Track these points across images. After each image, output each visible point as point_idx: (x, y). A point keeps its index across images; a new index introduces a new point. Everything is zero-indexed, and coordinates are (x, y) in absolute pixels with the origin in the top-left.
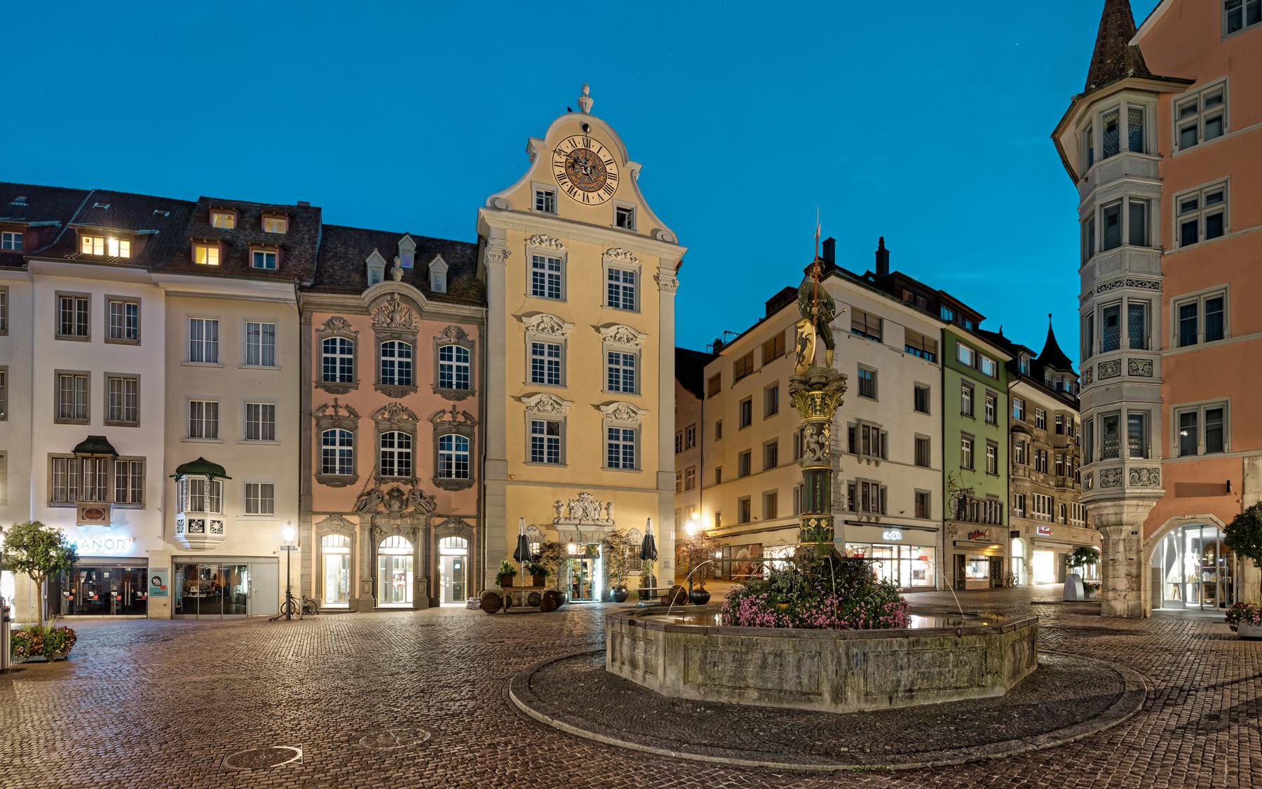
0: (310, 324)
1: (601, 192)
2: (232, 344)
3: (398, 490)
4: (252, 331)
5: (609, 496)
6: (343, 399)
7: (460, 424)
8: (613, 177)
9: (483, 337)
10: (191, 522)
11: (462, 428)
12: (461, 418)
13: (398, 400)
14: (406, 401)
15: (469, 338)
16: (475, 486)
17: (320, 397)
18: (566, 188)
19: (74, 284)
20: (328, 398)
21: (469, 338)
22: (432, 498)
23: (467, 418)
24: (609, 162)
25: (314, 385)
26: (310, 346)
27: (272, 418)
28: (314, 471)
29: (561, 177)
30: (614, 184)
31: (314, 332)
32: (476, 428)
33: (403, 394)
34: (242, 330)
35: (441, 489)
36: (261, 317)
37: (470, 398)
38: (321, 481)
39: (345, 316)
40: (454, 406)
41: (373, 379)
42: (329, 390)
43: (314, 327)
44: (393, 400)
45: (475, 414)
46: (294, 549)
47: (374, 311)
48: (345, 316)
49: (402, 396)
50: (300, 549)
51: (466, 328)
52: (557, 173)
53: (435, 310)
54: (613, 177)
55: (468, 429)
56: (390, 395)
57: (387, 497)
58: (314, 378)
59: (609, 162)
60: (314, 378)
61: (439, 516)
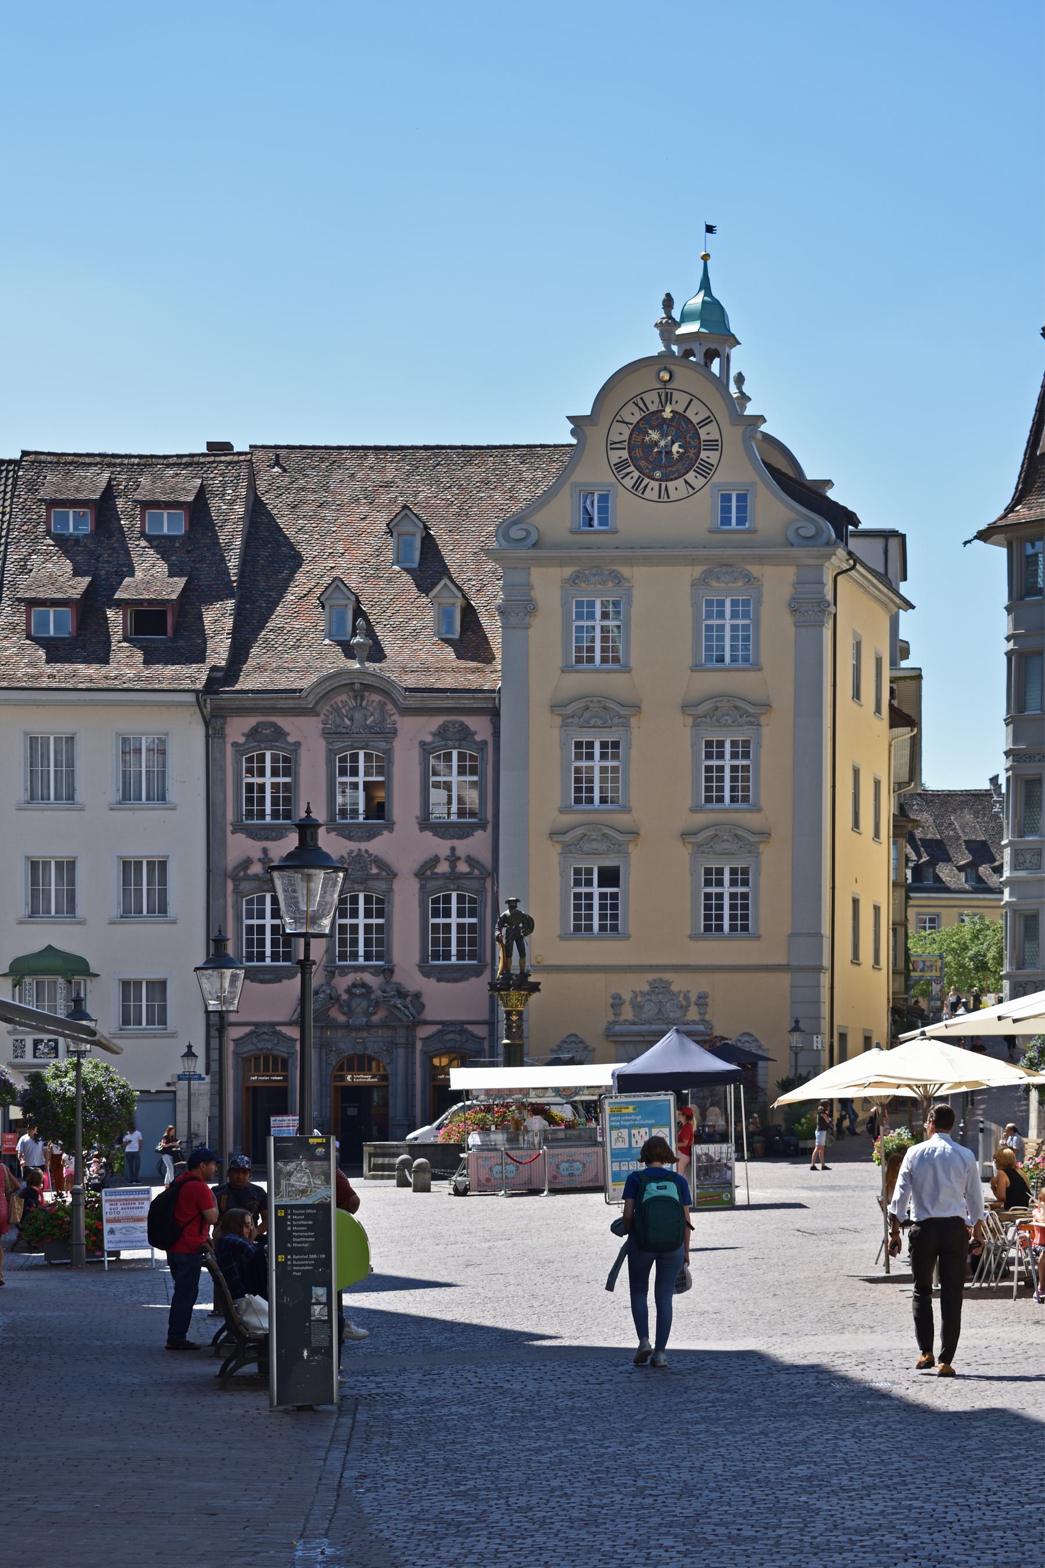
0: (223, 736)
1: (690, 476)
2: (97, 773)
3: (364, 985)
4: (128, 748)
7: (462, 876)
8: (713, 445)
10: (36, 1043)
11: (466, 883)
12: (463, 867)
13: (364, 846)
14: (375, 846)
15: (478, 738)
18: (629, 482)
21: (478, 738)
23: (470, 865)
24: (706, 422)
25: (230, 828)
26: (223, 769)
27: (163, 881)
29: (620, 466)
30: (713, 457)
31: (229, 747)
33: (371, 834)
34: (111, 751)
36: (144, 725)
40: (453, 849)
42: (254, 833)
43: (229, 740)
44: (353, 846)
46: (200, 1078)
49: (370, 837)
50: (208, 1079)
52: (614, 460)
54: (713, 445)
56: (350, 838)
58: (230, 817)
59: (706, 422)
61: (427, 1023)
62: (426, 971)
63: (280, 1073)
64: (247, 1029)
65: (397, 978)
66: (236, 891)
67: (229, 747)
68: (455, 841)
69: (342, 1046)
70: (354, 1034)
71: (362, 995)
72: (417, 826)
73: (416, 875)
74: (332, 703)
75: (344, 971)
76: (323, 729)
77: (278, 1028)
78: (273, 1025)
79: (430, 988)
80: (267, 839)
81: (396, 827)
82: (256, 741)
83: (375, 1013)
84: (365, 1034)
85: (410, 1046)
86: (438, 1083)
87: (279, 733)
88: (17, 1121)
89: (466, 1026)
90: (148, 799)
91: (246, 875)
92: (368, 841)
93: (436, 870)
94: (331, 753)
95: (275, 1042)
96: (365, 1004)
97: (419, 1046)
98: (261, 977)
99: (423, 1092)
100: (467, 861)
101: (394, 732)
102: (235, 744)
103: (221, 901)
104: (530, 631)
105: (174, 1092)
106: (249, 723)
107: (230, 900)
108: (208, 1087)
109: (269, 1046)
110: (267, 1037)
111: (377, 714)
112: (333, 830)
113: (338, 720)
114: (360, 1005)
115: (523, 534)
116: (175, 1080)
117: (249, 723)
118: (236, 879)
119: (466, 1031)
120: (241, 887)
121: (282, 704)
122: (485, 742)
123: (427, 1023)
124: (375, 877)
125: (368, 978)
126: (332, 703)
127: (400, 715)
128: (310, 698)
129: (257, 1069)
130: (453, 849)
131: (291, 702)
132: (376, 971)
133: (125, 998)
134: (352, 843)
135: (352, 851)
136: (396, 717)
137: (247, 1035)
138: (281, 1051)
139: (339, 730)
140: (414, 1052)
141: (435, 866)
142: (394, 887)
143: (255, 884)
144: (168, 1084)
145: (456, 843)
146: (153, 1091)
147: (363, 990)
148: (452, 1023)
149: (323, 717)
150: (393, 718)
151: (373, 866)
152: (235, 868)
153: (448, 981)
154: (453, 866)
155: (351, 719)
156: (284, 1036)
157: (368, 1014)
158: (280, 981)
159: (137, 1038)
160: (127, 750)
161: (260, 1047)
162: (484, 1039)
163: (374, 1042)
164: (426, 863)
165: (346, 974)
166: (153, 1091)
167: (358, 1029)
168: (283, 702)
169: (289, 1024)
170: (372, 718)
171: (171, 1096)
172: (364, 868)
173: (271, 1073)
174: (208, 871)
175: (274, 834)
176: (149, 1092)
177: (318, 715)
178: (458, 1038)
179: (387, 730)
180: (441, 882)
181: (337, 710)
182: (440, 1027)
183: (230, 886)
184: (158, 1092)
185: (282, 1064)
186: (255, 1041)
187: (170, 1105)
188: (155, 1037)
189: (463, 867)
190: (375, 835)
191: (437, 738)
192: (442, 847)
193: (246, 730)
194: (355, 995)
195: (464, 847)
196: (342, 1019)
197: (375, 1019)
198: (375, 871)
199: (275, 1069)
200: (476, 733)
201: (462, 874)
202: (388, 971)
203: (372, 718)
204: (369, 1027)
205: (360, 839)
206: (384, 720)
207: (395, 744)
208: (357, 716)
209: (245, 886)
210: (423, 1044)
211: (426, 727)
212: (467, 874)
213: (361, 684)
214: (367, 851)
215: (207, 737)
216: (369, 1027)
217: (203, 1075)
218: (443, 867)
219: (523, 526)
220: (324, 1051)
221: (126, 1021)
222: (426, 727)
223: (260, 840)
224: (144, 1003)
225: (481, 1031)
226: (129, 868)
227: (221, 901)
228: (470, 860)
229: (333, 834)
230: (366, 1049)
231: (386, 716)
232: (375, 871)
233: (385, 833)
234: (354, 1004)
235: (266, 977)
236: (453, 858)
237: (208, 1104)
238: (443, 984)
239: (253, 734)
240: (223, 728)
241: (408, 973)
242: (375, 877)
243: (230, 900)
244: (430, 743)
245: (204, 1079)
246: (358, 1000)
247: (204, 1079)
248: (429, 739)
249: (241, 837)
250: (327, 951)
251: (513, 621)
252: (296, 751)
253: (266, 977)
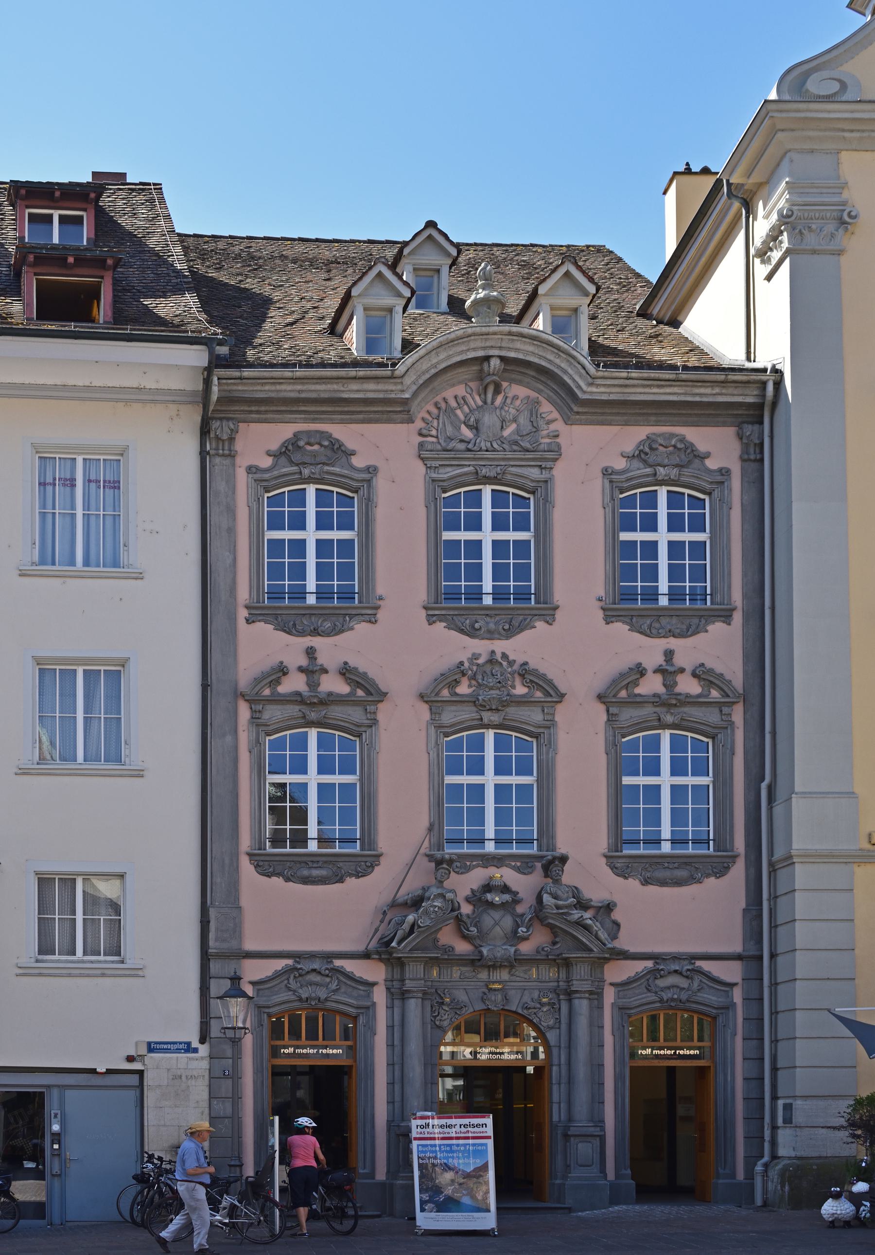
0: (232, 455)
5: (344, 381)
6: (331, 650)
9: (755, 456)
13: (500, 646)
14: (526, 647)
16: (738, 871)
17: (261, 647)
19: (535, 1061)
20: (290, 649)
21: (712, 464)
22: (609, 907)
25: (243, 613)
26: (231, 511)
28: (245, 842)
31: (242, 476)
32: (738, 715)
35: (633, 884)
37: (717, 628)
38: (267, 867)
39: (338, 431)
40: (669, 654)
41: (421, 593)
43: (242, 462)
44: (481, 647)
45: (732, 666)
47: (423, 410)
48: (338, 431)
49: (510, 633)
50: (204, 1050)
51: (699, 437)
53: (615, 395)
55: (712, 717)
56: (472, 632)
57: (466, 909)
58: (243, 594)
60: (243, 594)
61: (625, 955)
62: (621, 866)
63: (696, 1043)
64: (280, 964)
65: (569, 876)
66: (255, 719)
67: (242, 476)
68: (672, 640)
69: (462, 996)
70: (483, 975)
71: (503, 905)
72: (601, 614)
73: (601, 697)
74: (438, 398)
75: (462, 864)
76: (421, 445)
77: (338, 963)
78: (329, 957)
79: (630, 897)
80: (315, 632)
81: (559, 614)
82: (292, 463)
83: (526, 939)
84: (505, 975)
85: (596, 995)
86: (641, 1063)
87: (338, 451)
88: (304, 1206)
89: (699, 963)
90: (87, 562)
91: (274, 693)
92: (508, 638)
93: (637, 691)
94: (435, 485)
95: (334, 986)
96: (508, 922)
97: (609, 996)
98: (306, 872)
99: (618, 1078)
100: (694, 675)
101: (556, 452)
102: (251, 470)
103: (229, 739)
104: (843, 259)
105: (141, 1073)
106: (281, 432)
107: (244, 738)
108: (205, 1064)
109: (322, 993)
110: (317, 978)
111: (523, 420)
112: (441, 618)
113: (450, 430)
114: (499, 924)
115: (836, 86)
116: (143, 1050)
117: (281, 432)
118: (253, 701)
119: (700, 972)
120: (266, 716)
121: (353, 390)
122: (725, 472)
123: (625, 955)
124: (522, 701)
125: (506, 875)
126: (438, 398)
127: (567, 421)
128: (408, 380)
129: (653, 1037)
130: (669, 654)
131: (371, 386)
132: (525, 865)
133: (44, 905)
134: (476, 641)
135: (476, 656)
136: (559, 426)
137: (277, 975)
138: (346, 1000)
139: (452, 445)
140: (601, 1007)
141: (636, 683)
142: (557, 718)
143: (293, 710)
144: (130, 1059)
145: (673, 643)
146: (101, 1069)
147: (507, 897)
148: (676, 957)
149: (419, 424)
150: (553, 427)
151: (518, 681)
152: (257, 681)
153: (663, 883)
154: (669, 685)
155: (475, 428)
156: (350, 977)
157: (515, 937)
158: (341, 880)
159: (70, 975)
160: (49, 479)
161: (304, 996)
162: (732, 985)
163: (523, 988)
164: (622, 676)
165: (468, 869)
166: (101, 1069)
167: (494, 966)
168: (354, 386)
169: (366, 955)
170: (514, 426)
171: (134, 1080)
172: (501, 684)
173: (679, 1043)
174: (205, 687)
175: (328, 625)
176: (93, 1071)
177: (411, 421)
178: (683, 983)
179: (541, 447)
180: (648, 711)
181: (444, 410)
182: (650, 964)
183: (244, 712)
184: (109, 1072)
185: (711, 1021)
186: (293, 985)
187: (132, 1095)
188: (103, 975)
189: (688, 686)
190: (521, 629)
191: (636, 463)
192: (649, 651)
193: (275, 446)
194: (491, 905)
195: (689, 651)
196: (462, 947)
197: (526, 948)
198: (520, 690)
199: (329, 1036)
200: (708, 455)
201: (688, 696)
202: (553, 865)
203: (514, 426)
204: (514, 963)
205: (491, 635)
206: (537, 429)
207: (555, 472)
208: (489, 420)
209: (273, 714)
210: (618, 996)
211: (610, 445)
212: (699, 696)
213: (502, 358)
214: (504, 656)
215: (203, 454)
216: (514, 963)
217: (195, 1044)
218: (652, 685)
219: (835, 74)
220: (428, 1004)
221: (45, 948)
222: (610, 445)
223: (302, 634)
224: (79, 917)
225: (730, 972)
226: (52, 677)
227: (229, 739)
228: (701, 674)
229: (440, 626)
230: (506, 999)
231: (541, 423)
232: (520, 690)
233: (540, 625)
234: (487, 921)
235: (315, 873)
236: (668, 672)
237: (205, 1095)
238: (652, 889)
239: (287, 451)
240: (232, 440)
241: (589, 872)
242: (522, 701)
243: (244, 738)
244: (623, 472)
245: (196, 1050)
246: (497, 915)
247: (196, 1050)
248: (620, 464)
249: (264, 629)
250: (430, 829)
251: (811, 241)
252: (369, 481)
253: (315, 873)
